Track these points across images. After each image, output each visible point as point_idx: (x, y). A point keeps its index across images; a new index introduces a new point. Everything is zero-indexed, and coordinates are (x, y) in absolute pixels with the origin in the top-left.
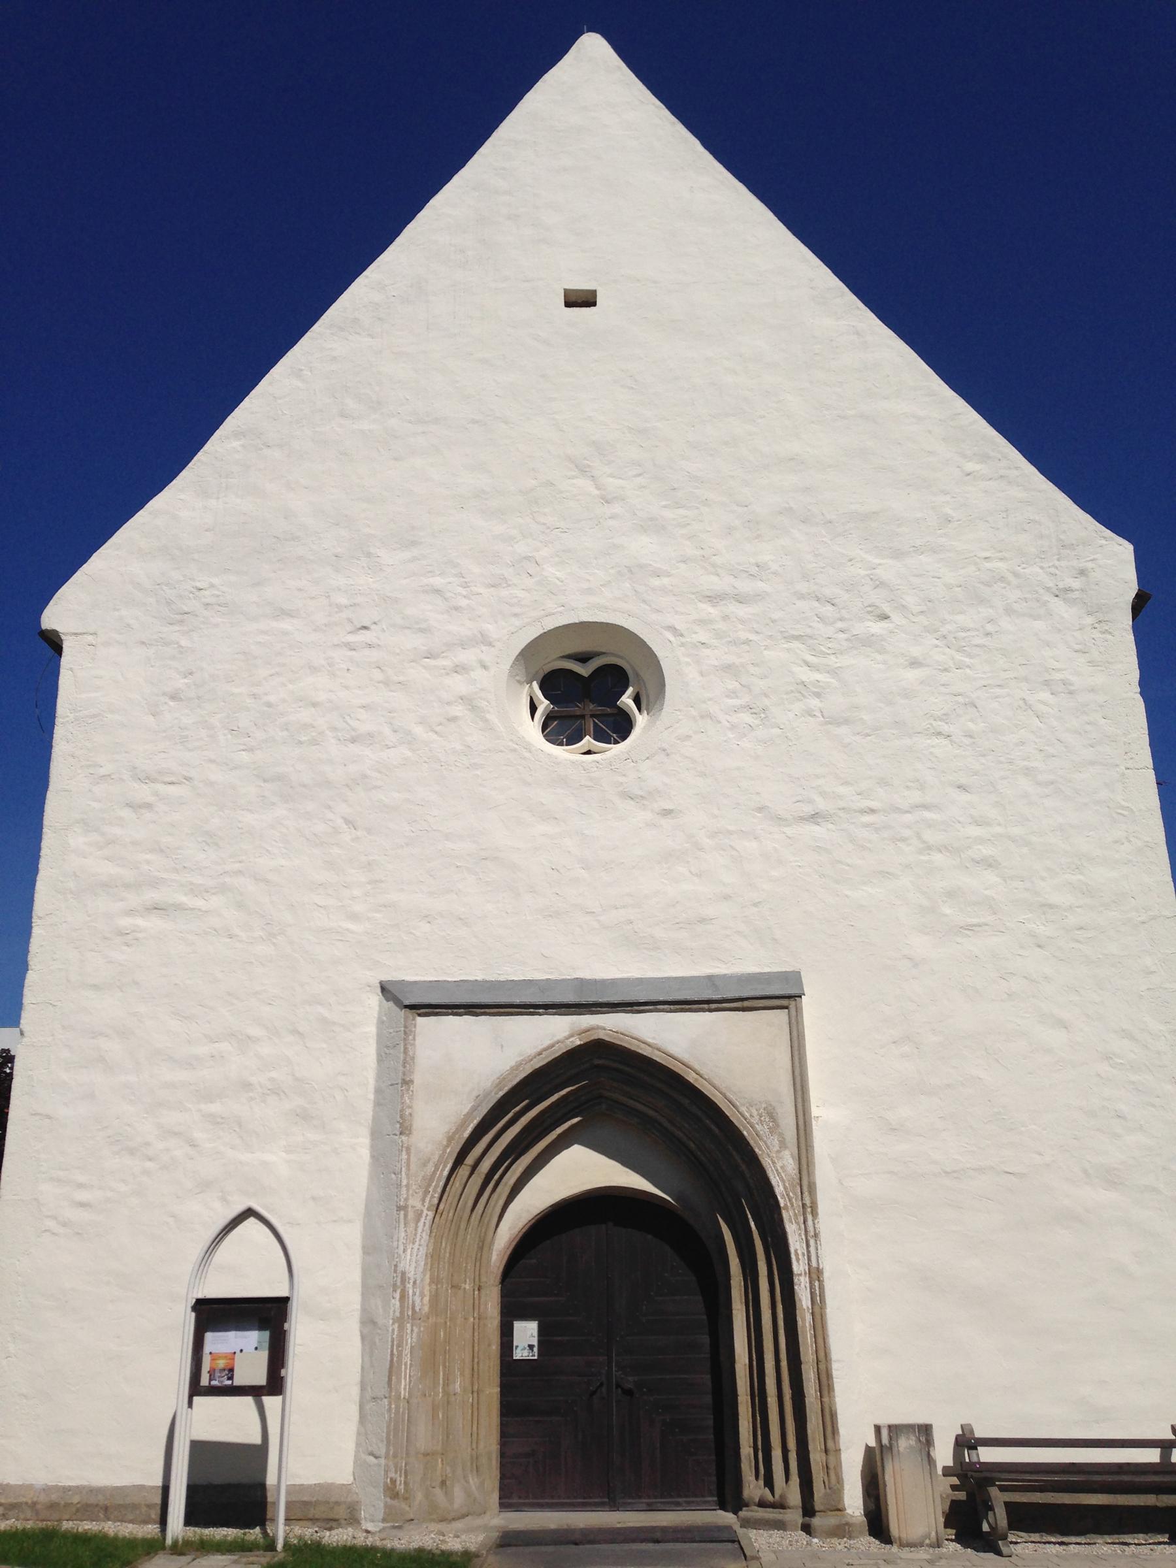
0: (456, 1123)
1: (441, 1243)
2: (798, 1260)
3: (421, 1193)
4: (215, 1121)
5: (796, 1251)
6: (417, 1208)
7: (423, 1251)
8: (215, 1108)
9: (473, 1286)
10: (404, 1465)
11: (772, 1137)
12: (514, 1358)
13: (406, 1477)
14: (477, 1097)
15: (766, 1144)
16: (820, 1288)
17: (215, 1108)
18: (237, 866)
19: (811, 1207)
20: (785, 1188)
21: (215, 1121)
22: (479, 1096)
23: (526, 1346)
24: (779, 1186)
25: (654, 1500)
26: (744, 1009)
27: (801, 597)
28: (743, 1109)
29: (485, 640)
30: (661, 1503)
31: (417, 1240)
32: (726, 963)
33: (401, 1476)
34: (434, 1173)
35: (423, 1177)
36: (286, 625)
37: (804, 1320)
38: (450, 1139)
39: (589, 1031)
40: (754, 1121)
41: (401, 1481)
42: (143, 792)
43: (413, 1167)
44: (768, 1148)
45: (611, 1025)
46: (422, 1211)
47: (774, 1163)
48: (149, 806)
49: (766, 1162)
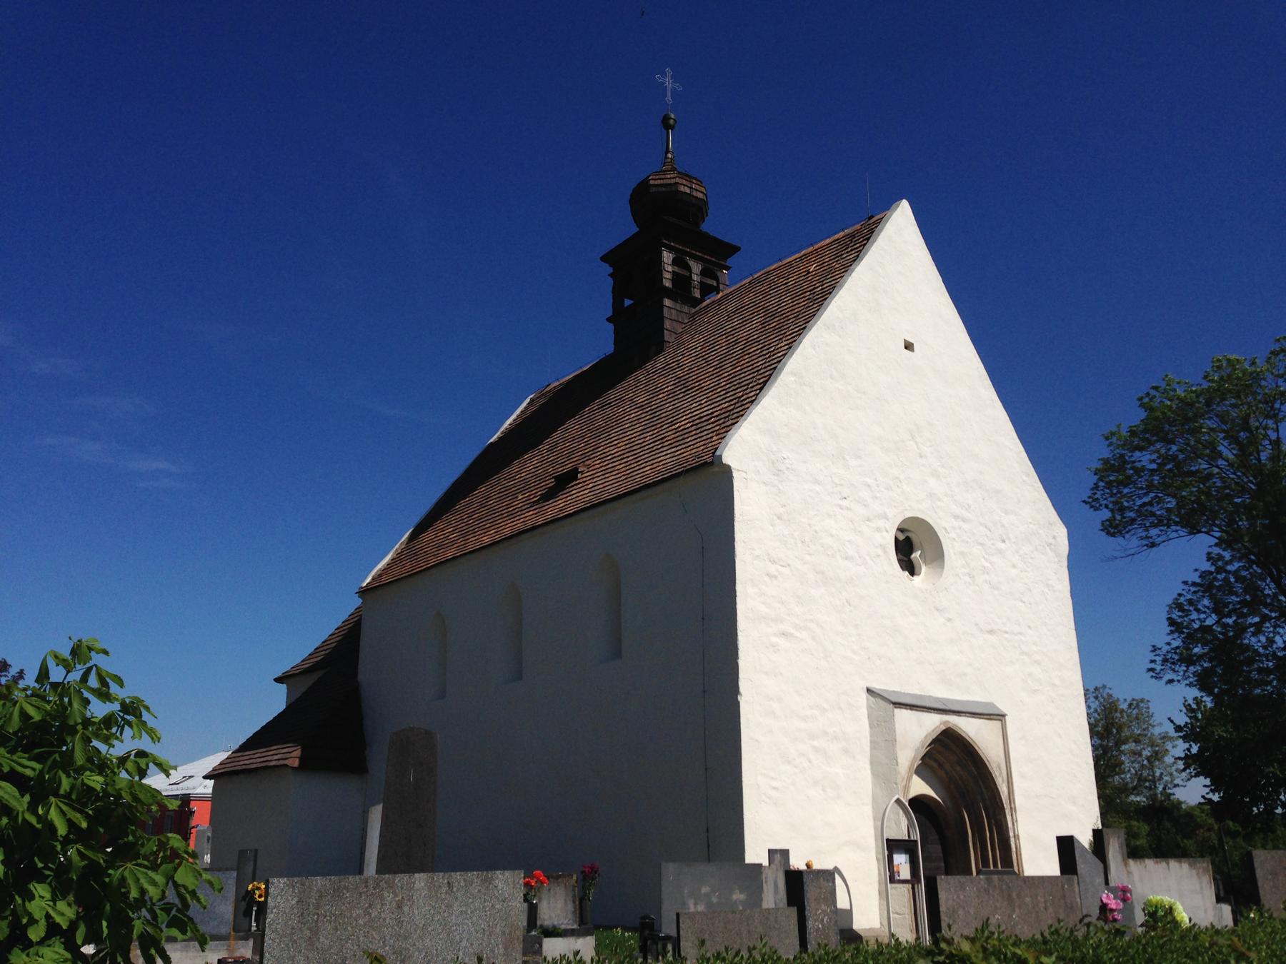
4: (816, 749)
8: (815, 743)
17: (815, 743)
18: (811, 617)
19: (18, 799)
21: (816, 749)
27: (981, 524)
29: (885, 517)
36: (817, 488)
42: (773, 569)
45: (954, 721)
48: (776, 577)
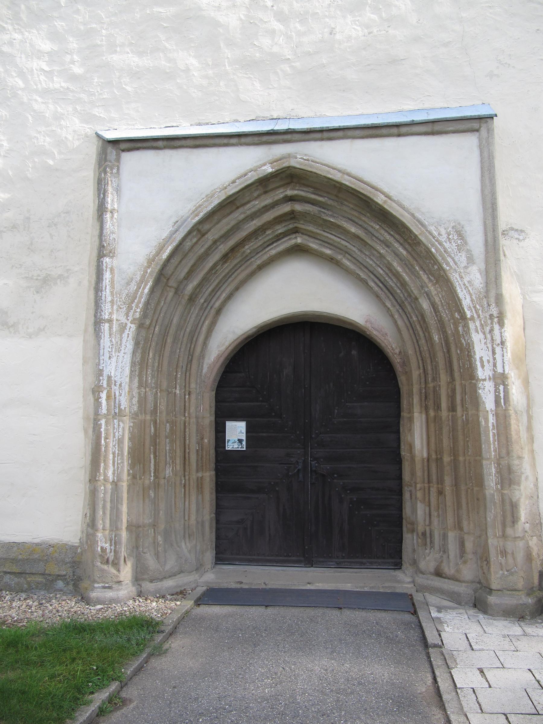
0: (155, 246)
1: (149, 353)
2: (483, 366)
3: (125, 308)
5: (481, 358)
6: (122, 322)
7: (128, 358)
9: (185, 392)
10: (113, 536)
11: (460, 254)
12: (227, 449)
13: (115, 547)
14: (175, 223)
15: (454, 260)
16: (504, 391)
20: (472, 300)
22: (177, 221)
23: (236, 440)
24: (465, 299)
25: (343, 560)
26: (433, 133)
28: (432, 228)
30: (348, 562)
31: (122, 349)
32: (416, 101)
33: (111, 545)
34: (137, 291)
35: (127, 295)
37: (487, 420)
38: (150, 261)
39: (280, 159)
40: (443, 238)
41: (111, 549)
43: (117, 287)
44: (456, 263)
46: (126, 324)
47: (461, 278)
49: (454, 277)
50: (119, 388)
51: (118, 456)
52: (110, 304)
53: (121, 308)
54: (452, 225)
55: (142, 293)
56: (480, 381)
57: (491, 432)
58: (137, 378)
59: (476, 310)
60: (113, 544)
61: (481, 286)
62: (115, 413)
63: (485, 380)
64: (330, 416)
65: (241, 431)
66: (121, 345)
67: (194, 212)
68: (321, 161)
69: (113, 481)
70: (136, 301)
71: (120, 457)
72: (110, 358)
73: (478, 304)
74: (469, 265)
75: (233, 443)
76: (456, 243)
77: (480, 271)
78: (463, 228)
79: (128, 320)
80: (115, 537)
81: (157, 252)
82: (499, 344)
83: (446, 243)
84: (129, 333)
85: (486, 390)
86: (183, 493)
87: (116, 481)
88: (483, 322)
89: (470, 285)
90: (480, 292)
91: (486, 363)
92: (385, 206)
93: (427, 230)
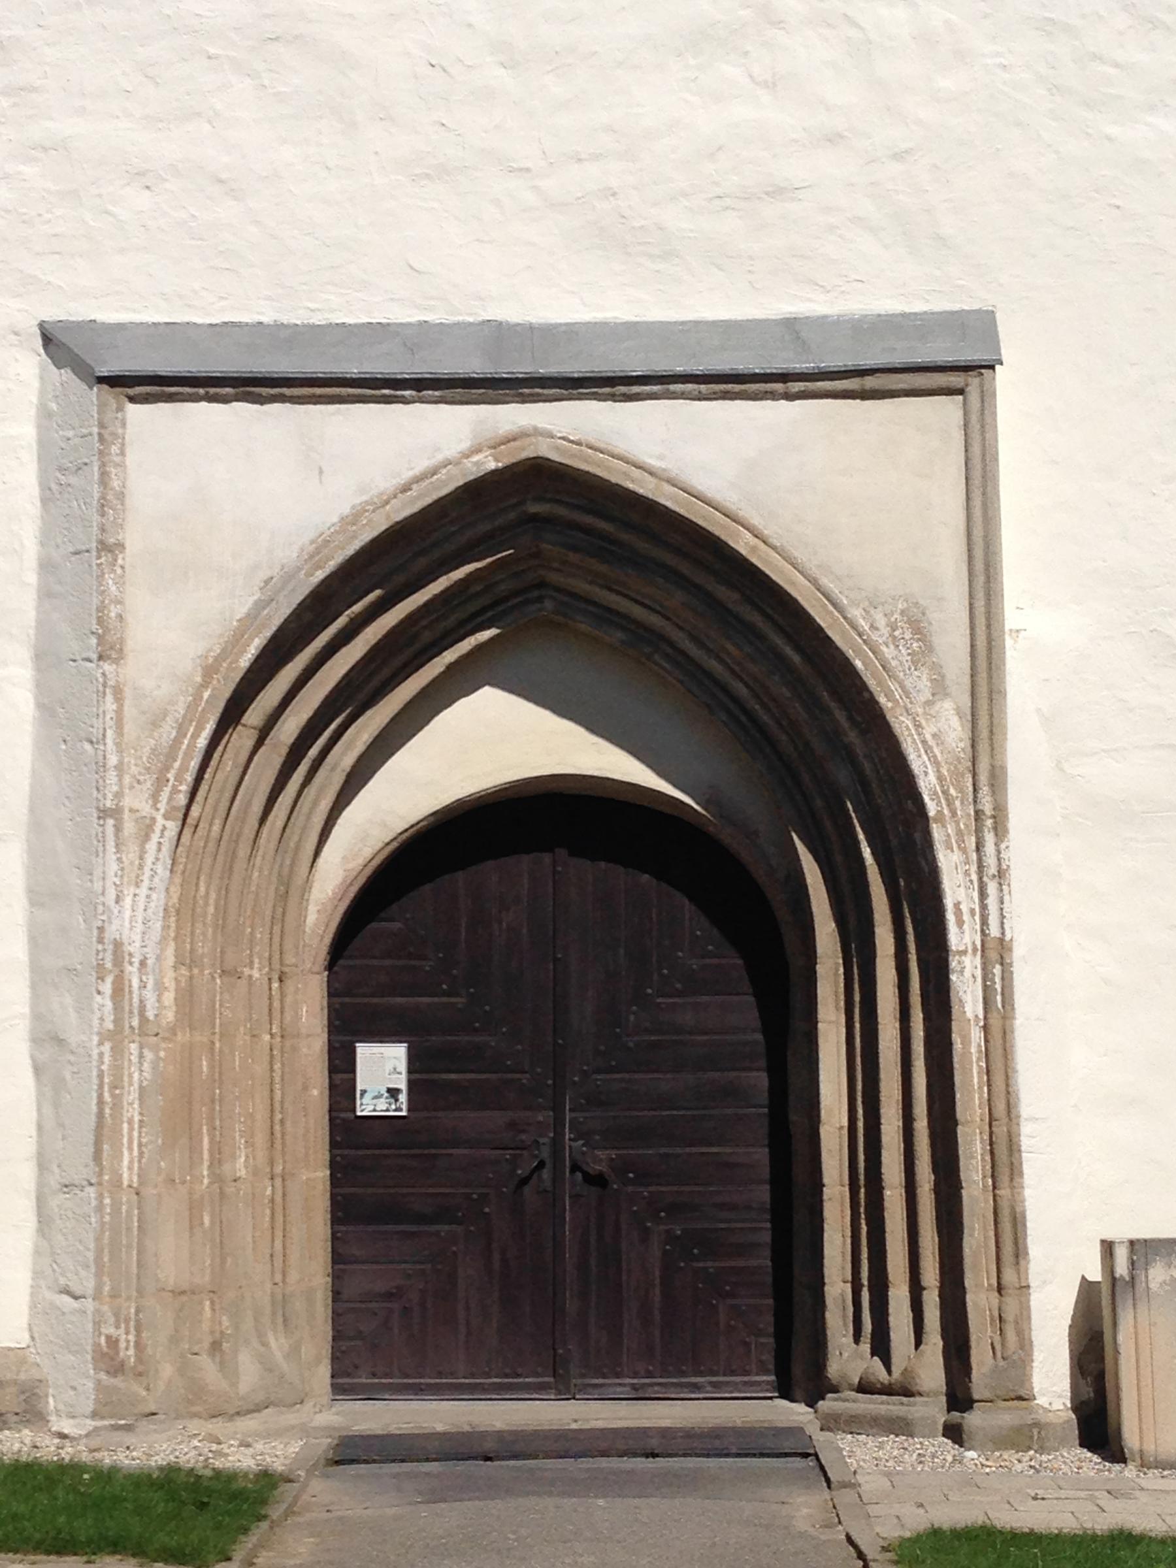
0: (221, 635)
1: (197, 885)
2: (960, 923)
3: (149, 784)
5: (957, 905)
10: (133, 1310)
12: (359, 1114)
14: (267, 582)
15: (903, 687)
16: (1003, 979)
20: (940, 778)
23: (384, 1091)
24: (926, 773)
28: (856, 613)
32: (828, 292)
33: (127, 1333)
34: (177, 741)
35: (153, 750)
37: (966, 1041)
41: (128, 1341)
43: (131, 729)
44: (907, 694)
46: (153, 820)
47: (918, 726)
50: (140, 970)
51: (140, 1127)
52: (115, 773)
53: (139, 782)
54: (900, 606)
55: (192, 745)
56: (954, 956)
57: (975, 1065)
58: (172, 944)
59: (947, 800)
60: (132, 1330)
61: (962, 745)
62: (131, 1027)
63: (964, 952)
64: (618, 1030)
65: (395, 1069)
66: (141, 867)
67: (311, 557)
68: (610, 448)
69: (130, 1186)
70: (177, 765)
71: (144, 1129)
72: (118, 900)
73: (953, 784)
74: (937, 697)
75: (375, 1097)
76: (908, 648)
77: (959, 713)
78: (924, 614)
79: (158, 810)
80: (137, 1312)
81: (224, 650)
82: (994, 876)
83: (887, 646)
84: (162, 840)
85: (967, 973)
86: (267, 1219)
87: (135, 1185)
88: (962, 826)
89: (938, 744)
90: (958, 759)
91: (966, 917)
92: (754, 560)
93: (845, 618)
